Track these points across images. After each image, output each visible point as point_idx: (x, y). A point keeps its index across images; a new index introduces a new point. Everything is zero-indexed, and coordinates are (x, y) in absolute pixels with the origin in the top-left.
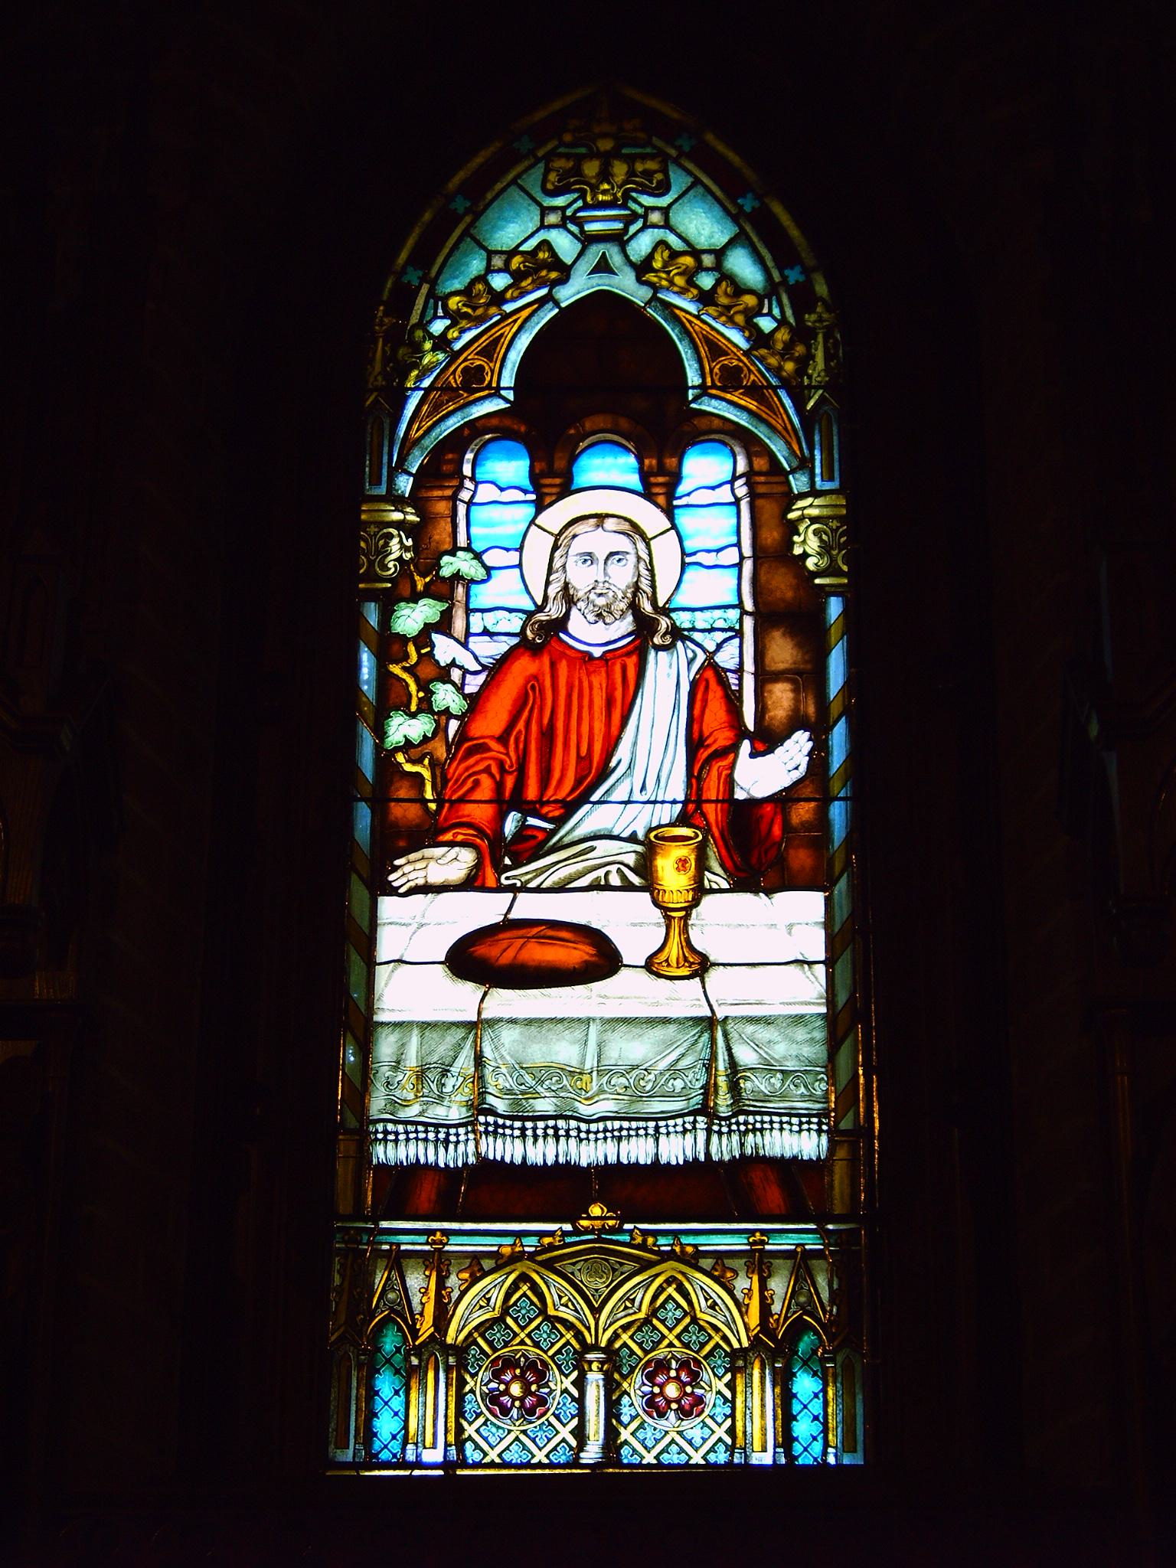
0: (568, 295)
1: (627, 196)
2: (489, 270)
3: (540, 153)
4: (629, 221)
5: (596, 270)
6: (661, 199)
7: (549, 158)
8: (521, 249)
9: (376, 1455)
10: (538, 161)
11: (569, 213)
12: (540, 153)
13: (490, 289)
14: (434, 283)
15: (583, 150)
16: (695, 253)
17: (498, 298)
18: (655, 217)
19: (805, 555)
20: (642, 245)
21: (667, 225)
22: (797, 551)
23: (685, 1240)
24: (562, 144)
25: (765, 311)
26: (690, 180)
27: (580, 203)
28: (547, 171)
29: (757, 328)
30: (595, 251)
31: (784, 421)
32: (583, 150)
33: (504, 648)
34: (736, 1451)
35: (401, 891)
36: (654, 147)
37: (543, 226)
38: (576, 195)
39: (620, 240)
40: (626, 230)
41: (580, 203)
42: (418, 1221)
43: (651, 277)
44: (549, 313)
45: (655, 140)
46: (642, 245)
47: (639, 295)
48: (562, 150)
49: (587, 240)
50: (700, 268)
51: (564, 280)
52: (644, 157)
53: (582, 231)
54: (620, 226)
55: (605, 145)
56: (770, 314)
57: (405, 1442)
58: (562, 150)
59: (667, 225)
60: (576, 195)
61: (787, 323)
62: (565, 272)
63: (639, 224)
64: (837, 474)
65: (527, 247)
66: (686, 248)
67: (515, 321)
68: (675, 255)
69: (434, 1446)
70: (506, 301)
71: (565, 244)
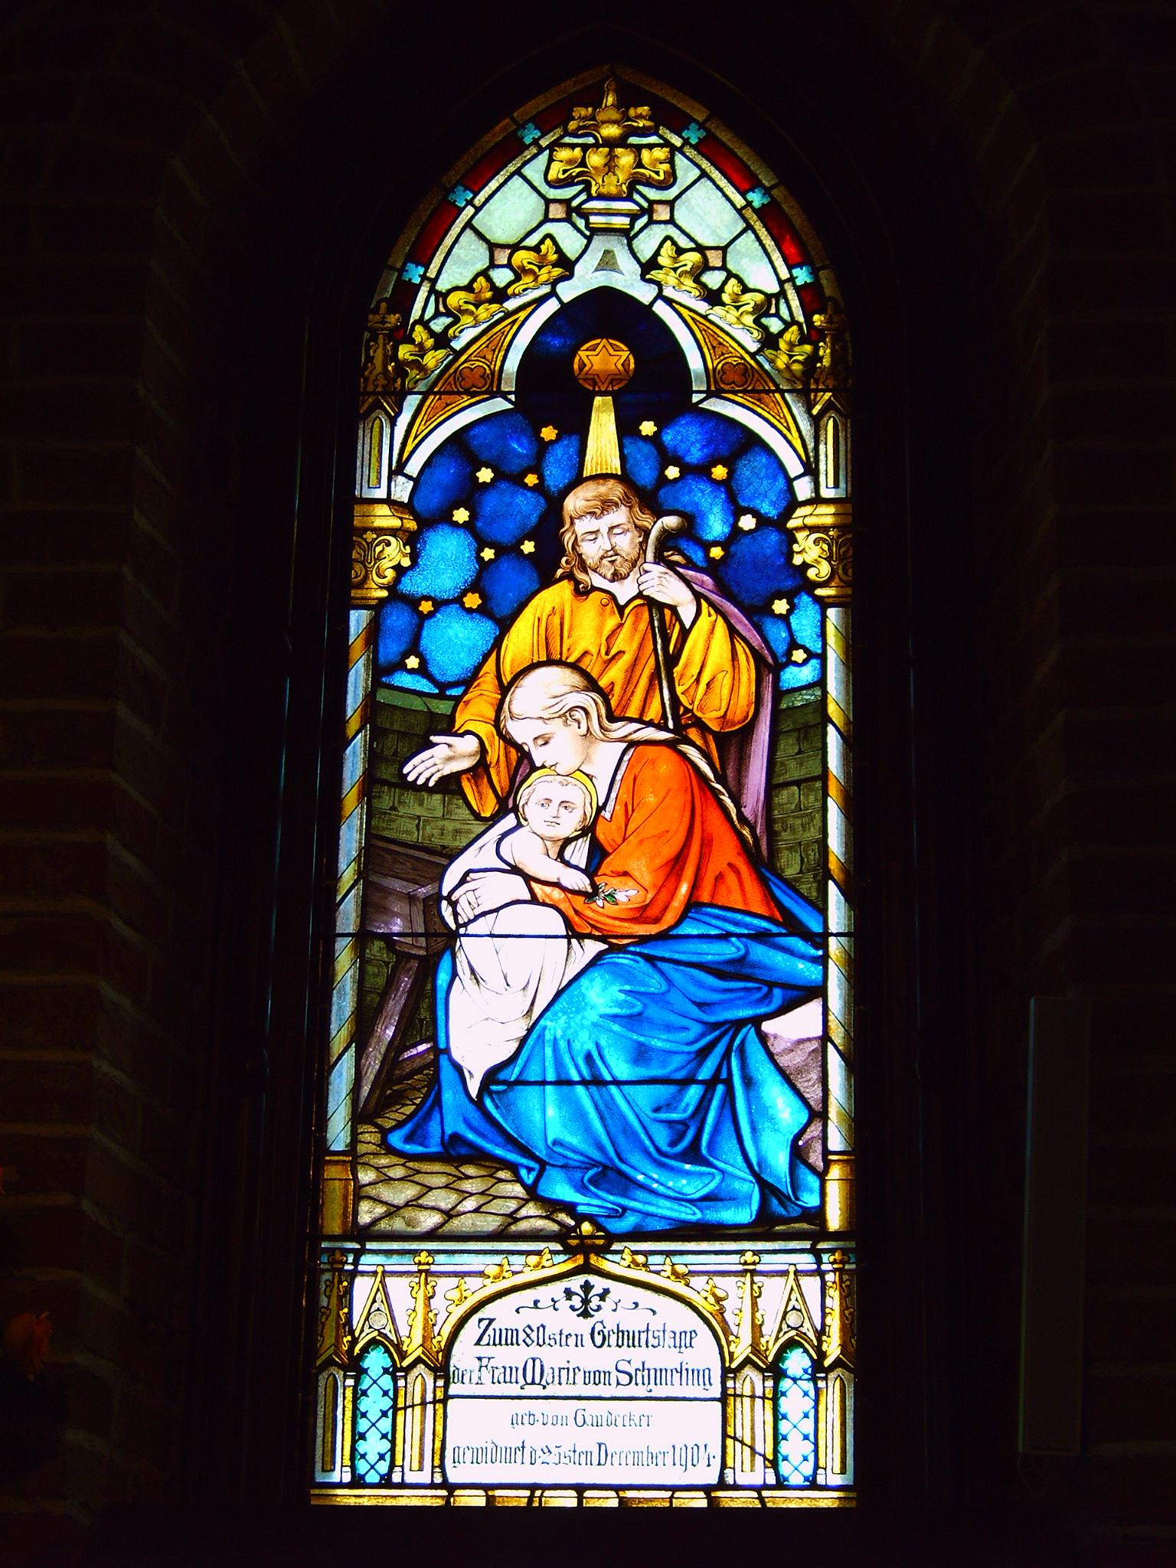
0: (568, 291)
1: (632, 188)
2: (493, 265)
3: (544, 143)
4: (634, 217)
5: (599, 268)
6: (666, 192)
7: (552, 147)
8: (524, 244)
9: (362, 1477)
10: (541, 150)
11: (575, 203)
12: (544, 143)
13: (493, 286)
14: (434, 281)
15: (591, 140)
16: (700, 249)
17: (500, 295)
18: (662, 213)
19: (806, 566)
20: (646, 245)
21: (671, 221)
22: (797, 560)
23: (676, 1259)
24: (567, 133)
25: (773, 311)
26: (697, 173)
27: (583, 197)
28: (551, 160)
29: (765, 329)
30: (599, 244)
31: (786, 421)
32: (591, 140)
33: (421, 708)
34: (422, 953)
35: (652, 1268)
36: (661, 137)
37: (546, 219)
38: (580, 187)
39: (628, 235)
40: (632, 224)
41: (583, 197)
42: (338, 838)
43: (655, 274)
44: (551, 307)
45: (662, 130)
46: (646, 245)
47: (644, 293)
48: (567, 140)
49: (592, 233)
50: (706, 267)
51: (568, 276)
52: (651, 147)
53: (587, 223)
54: (627, 220)
55: (612, 131)
56: (777, 315)
57: (392, 1465)
58: (567, 140)
59: (671, 221)
60: (580, 187)
61: (794, 322)
62: (567, 266)
63: (644, 220)
64: (842, 485)
65: (532, 241)
66: (692, 245)
67: (514, 322)
68: (680, 251)
69: (421, 1469)
70: (508, 298)
71: (570, 240)
